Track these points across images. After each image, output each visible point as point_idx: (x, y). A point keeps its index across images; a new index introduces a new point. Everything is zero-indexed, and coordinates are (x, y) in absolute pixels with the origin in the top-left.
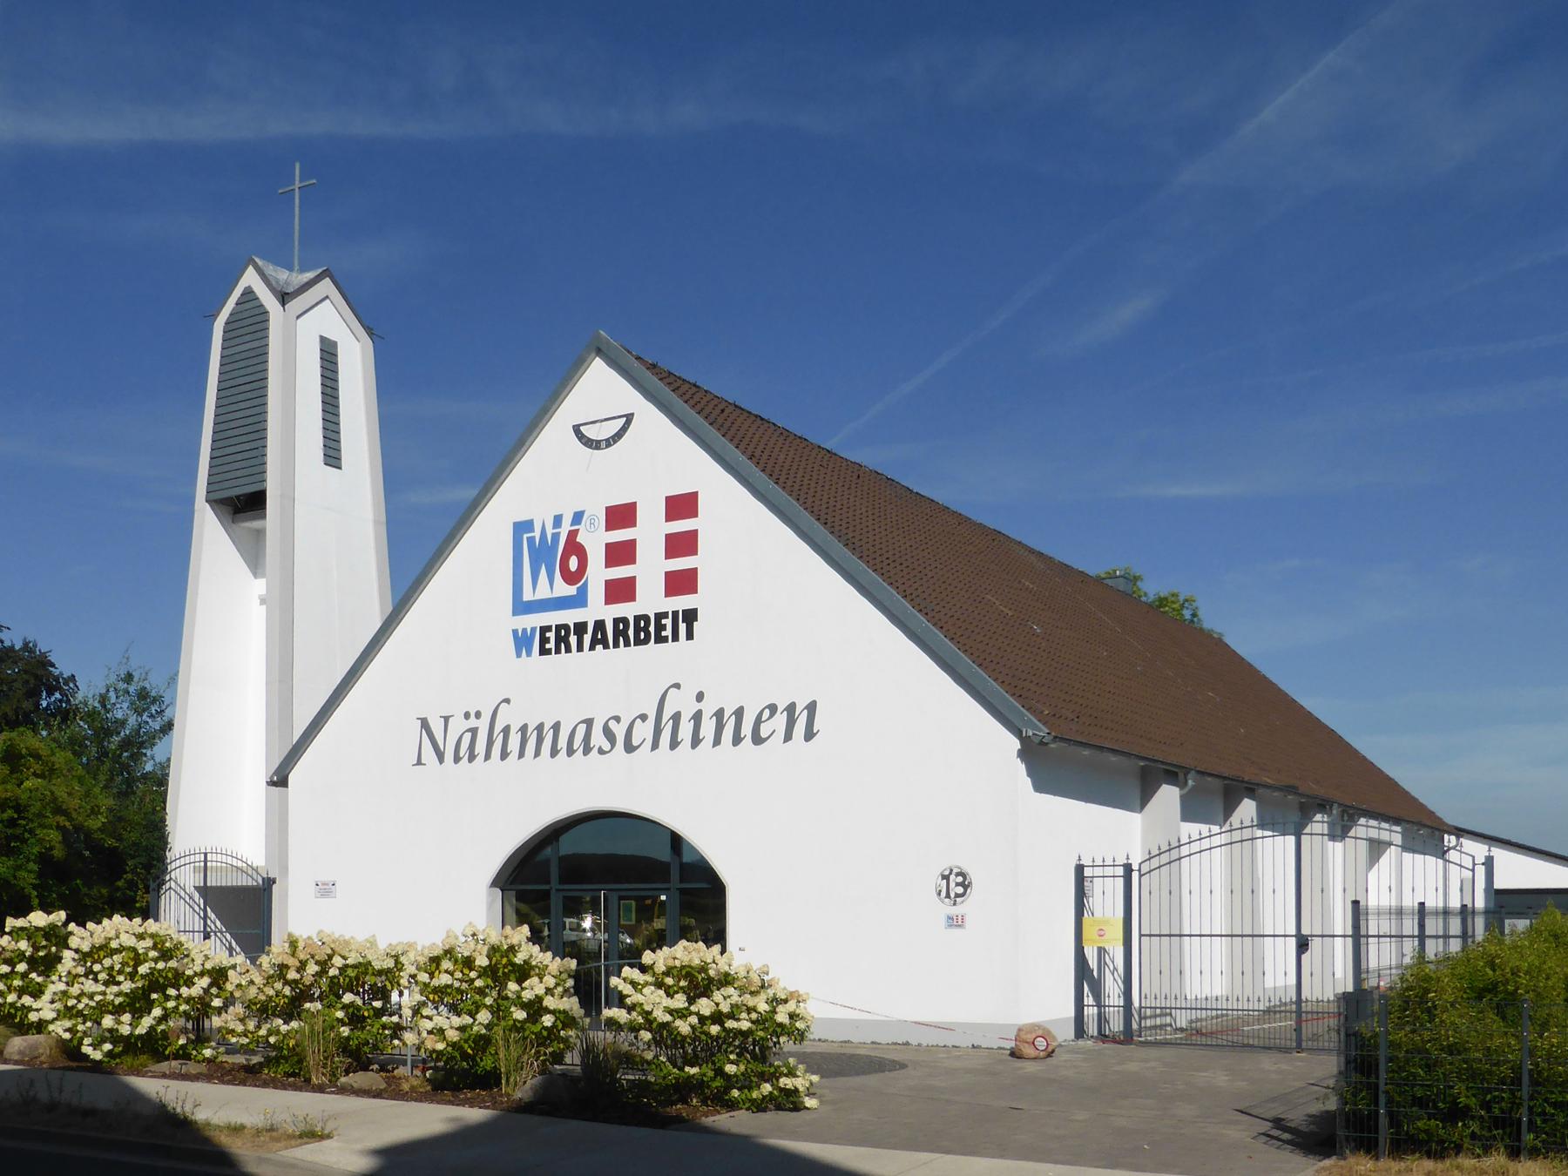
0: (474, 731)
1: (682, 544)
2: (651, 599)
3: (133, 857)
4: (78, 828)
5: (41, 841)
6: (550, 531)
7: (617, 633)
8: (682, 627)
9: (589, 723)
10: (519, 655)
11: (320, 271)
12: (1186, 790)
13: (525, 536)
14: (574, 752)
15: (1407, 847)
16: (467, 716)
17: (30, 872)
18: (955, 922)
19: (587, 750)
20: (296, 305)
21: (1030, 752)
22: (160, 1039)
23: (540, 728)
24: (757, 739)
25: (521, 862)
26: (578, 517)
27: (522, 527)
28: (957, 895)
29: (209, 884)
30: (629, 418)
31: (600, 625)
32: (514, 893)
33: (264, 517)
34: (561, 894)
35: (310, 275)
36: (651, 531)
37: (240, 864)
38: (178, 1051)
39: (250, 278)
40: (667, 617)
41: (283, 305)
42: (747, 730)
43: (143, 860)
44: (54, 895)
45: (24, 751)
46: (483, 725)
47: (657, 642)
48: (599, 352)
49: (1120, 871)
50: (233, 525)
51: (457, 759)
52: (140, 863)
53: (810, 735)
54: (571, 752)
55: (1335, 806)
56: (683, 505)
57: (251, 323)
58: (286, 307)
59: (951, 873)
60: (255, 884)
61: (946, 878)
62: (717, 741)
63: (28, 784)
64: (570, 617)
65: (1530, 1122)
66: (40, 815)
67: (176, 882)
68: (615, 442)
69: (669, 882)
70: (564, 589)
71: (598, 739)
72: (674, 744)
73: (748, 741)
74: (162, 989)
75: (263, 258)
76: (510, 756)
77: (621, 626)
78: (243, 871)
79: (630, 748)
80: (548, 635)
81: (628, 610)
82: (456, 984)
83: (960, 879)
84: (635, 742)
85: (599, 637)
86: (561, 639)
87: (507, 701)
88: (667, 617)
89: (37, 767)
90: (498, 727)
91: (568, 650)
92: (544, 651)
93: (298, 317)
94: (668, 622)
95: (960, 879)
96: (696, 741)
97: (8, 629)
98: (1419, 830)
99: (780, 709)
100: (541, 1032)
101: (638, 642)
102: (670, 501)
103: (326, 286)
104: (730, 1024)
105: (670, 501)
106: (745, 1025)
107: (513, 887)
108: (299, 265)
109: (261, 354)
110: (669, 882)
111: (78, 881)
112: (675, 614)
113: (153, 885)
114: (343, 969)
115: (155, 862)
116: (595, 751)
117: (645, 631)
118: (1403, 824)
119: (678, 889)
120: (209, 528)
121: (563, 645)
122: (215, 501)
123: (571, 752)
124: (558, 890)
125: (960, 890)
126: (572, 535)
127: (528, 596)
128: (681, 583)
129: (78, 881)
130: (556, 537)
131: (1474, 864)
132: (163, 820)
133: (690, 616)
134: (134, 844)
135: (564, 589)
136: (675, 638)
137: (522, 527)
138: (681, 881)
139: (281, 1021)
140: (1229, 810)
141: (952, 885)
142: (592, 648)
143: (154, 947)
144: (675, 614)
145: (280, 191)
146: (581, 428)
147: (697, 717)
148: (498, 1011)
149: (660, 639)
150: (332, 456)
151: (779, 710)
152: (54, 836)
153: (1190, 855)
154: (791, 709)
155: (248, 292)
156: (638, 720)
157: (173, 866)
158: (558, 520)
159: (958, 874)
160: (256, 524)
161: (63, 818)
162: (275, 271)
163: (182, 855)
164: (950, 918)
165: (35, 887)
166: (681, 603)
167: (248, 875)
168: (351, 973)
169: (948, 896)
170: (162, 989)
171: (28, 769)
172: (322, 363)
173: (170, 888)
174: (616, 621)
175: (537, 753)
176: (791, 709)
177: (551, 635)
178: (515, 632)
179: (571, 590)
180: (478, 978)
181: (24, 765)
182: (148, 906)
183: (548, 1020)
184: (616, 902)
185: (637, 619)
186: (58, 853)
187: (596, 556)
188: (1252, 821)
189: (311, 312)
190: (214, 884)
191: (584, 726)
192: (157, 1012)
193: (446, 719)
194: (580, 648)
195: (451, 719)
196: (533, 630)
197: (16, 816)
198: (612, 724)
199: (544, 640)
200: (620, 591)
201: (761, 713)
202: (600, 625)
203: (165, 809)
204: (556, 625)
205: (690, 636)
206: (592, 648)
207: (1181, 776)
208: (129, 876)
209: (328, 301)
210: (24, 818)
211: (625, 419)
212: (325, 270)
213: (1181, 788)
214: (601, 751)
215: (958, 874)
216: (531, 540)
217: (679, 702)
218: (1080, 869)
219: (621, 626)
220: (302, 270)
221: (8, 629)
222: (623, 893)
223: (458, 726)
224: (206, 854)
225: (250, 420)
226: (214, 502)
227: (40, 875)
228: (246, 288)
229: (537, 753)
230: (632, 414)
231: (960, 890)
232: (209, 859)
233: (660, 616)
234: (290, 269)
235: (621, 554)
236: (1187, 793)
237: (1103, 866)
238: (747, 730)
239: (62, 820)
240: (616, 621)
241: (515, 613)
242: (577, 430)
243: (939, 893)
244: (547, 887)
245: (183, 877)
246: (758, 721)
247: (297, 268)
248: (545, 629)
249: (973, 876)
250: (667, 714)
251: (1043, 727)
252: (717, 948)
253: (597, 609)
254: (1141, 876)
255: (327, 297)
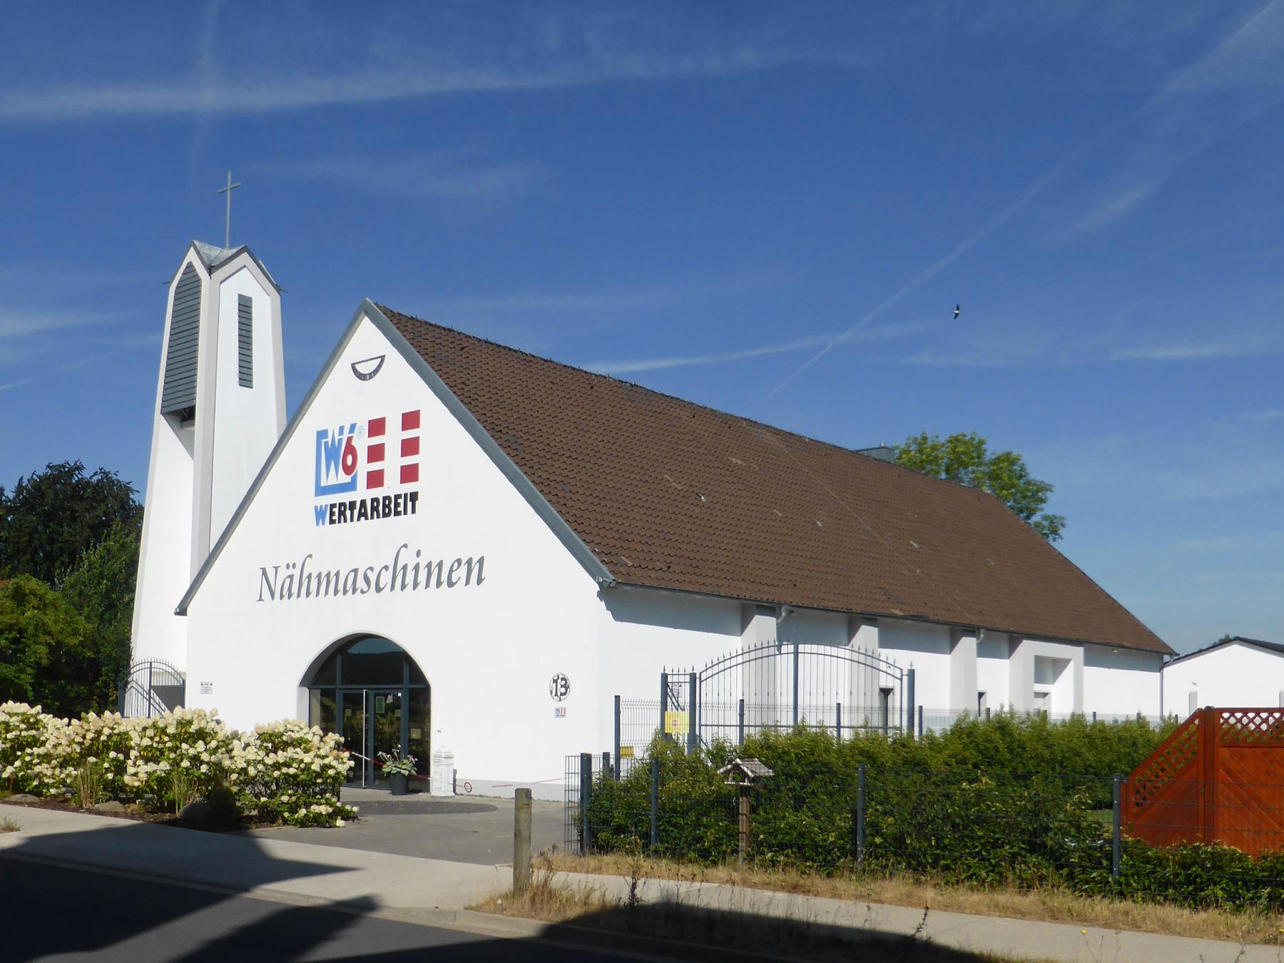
0: (291, 577)
1: (410, 447)
2: (393, 486)
3: (107, 665)
4: (59, 644)
5: (35, 653)
6: (337, 438)
7: (374, 509)
8: (409, 504)
9: (355, 571)
10: (318, 524)
11: (241, 247)
12: (781, 619)
13: (323, 441)
14: (381, 589)
15: (1088, 662)
16: (288, 566)
17: (29, 674)
18: (560, 713)
19: (354, 591)
20: (219, 274)
21: (606, 593)
22: (20, 781)
23: (328, 575)
24: (451, 584)
25: (319, 670)
26: (353, 427)
27: (322, 435)
28: (562, 694)
29: (152, 684)
30: (383, 358)
31: (363, 503)
32: (319, 691)
33: (193, 424)
34: (343, 692)
35: (234, 251)
36: (393, 437)
37: (170, 670)
38: (33, 789)
39: (192, 257)
40: (401, 498)
41: (210, 274)
42: (444, 577)
43: (112, 667)
44: (47, 691)
45: (27, 592)
46: (296, 572)
47: (395, 515)
48: (367, 313)
49: (688, 678)
50: (181, 430)
51: (282, 597)
52: (111, 669)
53: (480, 581)
54: (345, 592)
55: (982, 631)
56: (411, 420)
57: (190, 288)
58: (212, 276)
59: (558, 679)
60: (179, 684)
61: (555, 681)
62: (427, 585)
63: (28, 614)
64: (346, 497)
65: (657, 835)
66: (34, 635)
67: (136, 683)
68: (375, 375)
69: (403, 684)
70: (345, 478)
71: (361, 584)
72: (403, 587)
73: (445, 584)
74: (22, 750)
75: (200, 240)
76: (407, 587)
77: (375, 504)
78: (171, 675)
79: (451, 584)
80: (399, 501)
81: (379, 493)
82: (155, 745)
83: (563, 683)
84: (381, 586)
85: (363, 511)
86: (340, 513)
87: (310, 556)
88: (401, 498)
89: (35, 602)
90: (305, 575)
91: (345, 521)
92: (332, 522)
93: (221, 283)
94: (401, 501)
95: (563, 683)
96: (416, 585)
97: (138, 492)
98: (1114, 650)
99: (464, 562)
100: (200, 776)
101: (385, 515)
102: (405, 416)
103: (245, 256)
104: (284, 770)
105: (405, 416)
106: (292, 771)
107: (317, 686)
108: (230, 243)
109: (195, 309)
110: (403, 684)
111: (62, 681)
112: (406, 495)
113: (120, 685)
114: (109, 736)
115: (121, 669)
116: (359, 591)
117: (386, 508)
118: (1087, 645)
119: (408, 688)
120: (163, 431)
121: (342, 517)
122: (168, 413)
123: (345, 592)
124: (340, 689)
125: (563, 690)
126: (350, 439)
127: (323, 483)
128: (409, 474)
129: (62, 681)
130: (340, 441)
131: (902, 675)
132: (129, 639)
133: (414, 497)
134: (108, 656)
135: (345, 478)
136: (405, 512)
137: (322, 435)
138: (410, 683)
139: (72, 769)
140: (851, 633)
141: (559, 686)
142: (358, 520)
143: (23, 722)
144: (406, 495)
145: (220, 191)
146: (356, 365)
147: (417, 568)
148: (175, 763)
149: (397, 513)
150: (246, 379)
151: (463, 564)
152: (43, 650)
153: (730, 668)
154: (469, 562)
155: (190, 266)
156: (369, 570)
157: (135, 669)
158: (342, 429)
159: (562, 679)
160: (190, 429)
161: (49, 637)
162: (210, 250)
163: (721, 659)
164: (557, 710)
165: (31, 685)
166: (409, 488)
167: (171, 675)
168: (115, 738)
169: (556, 695)
170: (22, 750)
171: (29, 603)
172: (239, 313)
173: (132, 687)
174: (373, 500)
175: (326, 593)
176: (469, 562)
177: (336, 510)
178: (316, 507)
179: (347, 479)
180: (166, 742)
181: (27, 601)
182: (117, 699)
183: (204, 768)
184: (373, 697)
185: (385, 498)
186: (45, 662)
187: (362, 454)
188: (775, 642)
189: (233, 277)
190: (155, 685)
191: (353, 574)
192: (18, 763)
193: (276, 568)
194: (352, 520)
195: (279, 568)
196: (326, 506)
197: (18, 636)
198: (369, 572)
199: (332, 514)
200: (375, 479)
201: (453, 565)
202: (363, 503)
203: (131, 631)
204: (411, 493)
205: (413, 511)
206: (358, 520)
207: (777, 610)
208: (104, 678)
209: (245, 269)
210: (24, 637)
211: (380, 359)
212: (243, 248)
213: (777, 619)
214: (363, 592)
215: (562, 679)
216: (326, 443)
217: (408, 558)
218: (665, 676)
219: (375, 504)
220: (231, 247)
221: (138, 492)
222: (380, 692)
223: (283, 573)
224: (151, 663)
225: (187, 357)
226: (167, 414)
227: (35, 676)
228: (188, 263)
229: (326, 593)
230: (384, 356)
231: (563, 690)
232: (153, 666)
233: (397, 497)
234: (223, 246)
235: (376, 453)
236: (783, 621)
237: (679, 675)
238: (444, 577)
239: (48, 638)
240: (373, 500)
241: (316, 495)
242: (353, 366)
243: (551, 692)
244: (334, 687)
245: (139, 678)
246: (451, 571)
247: (228, 245)
248: (333, 506)
249: (571, 683)
250: (400, 566)
251: (610, 575)
252: (118, 714)
253: (363, 493)
254: (701, 682)
255: (245, 266)
